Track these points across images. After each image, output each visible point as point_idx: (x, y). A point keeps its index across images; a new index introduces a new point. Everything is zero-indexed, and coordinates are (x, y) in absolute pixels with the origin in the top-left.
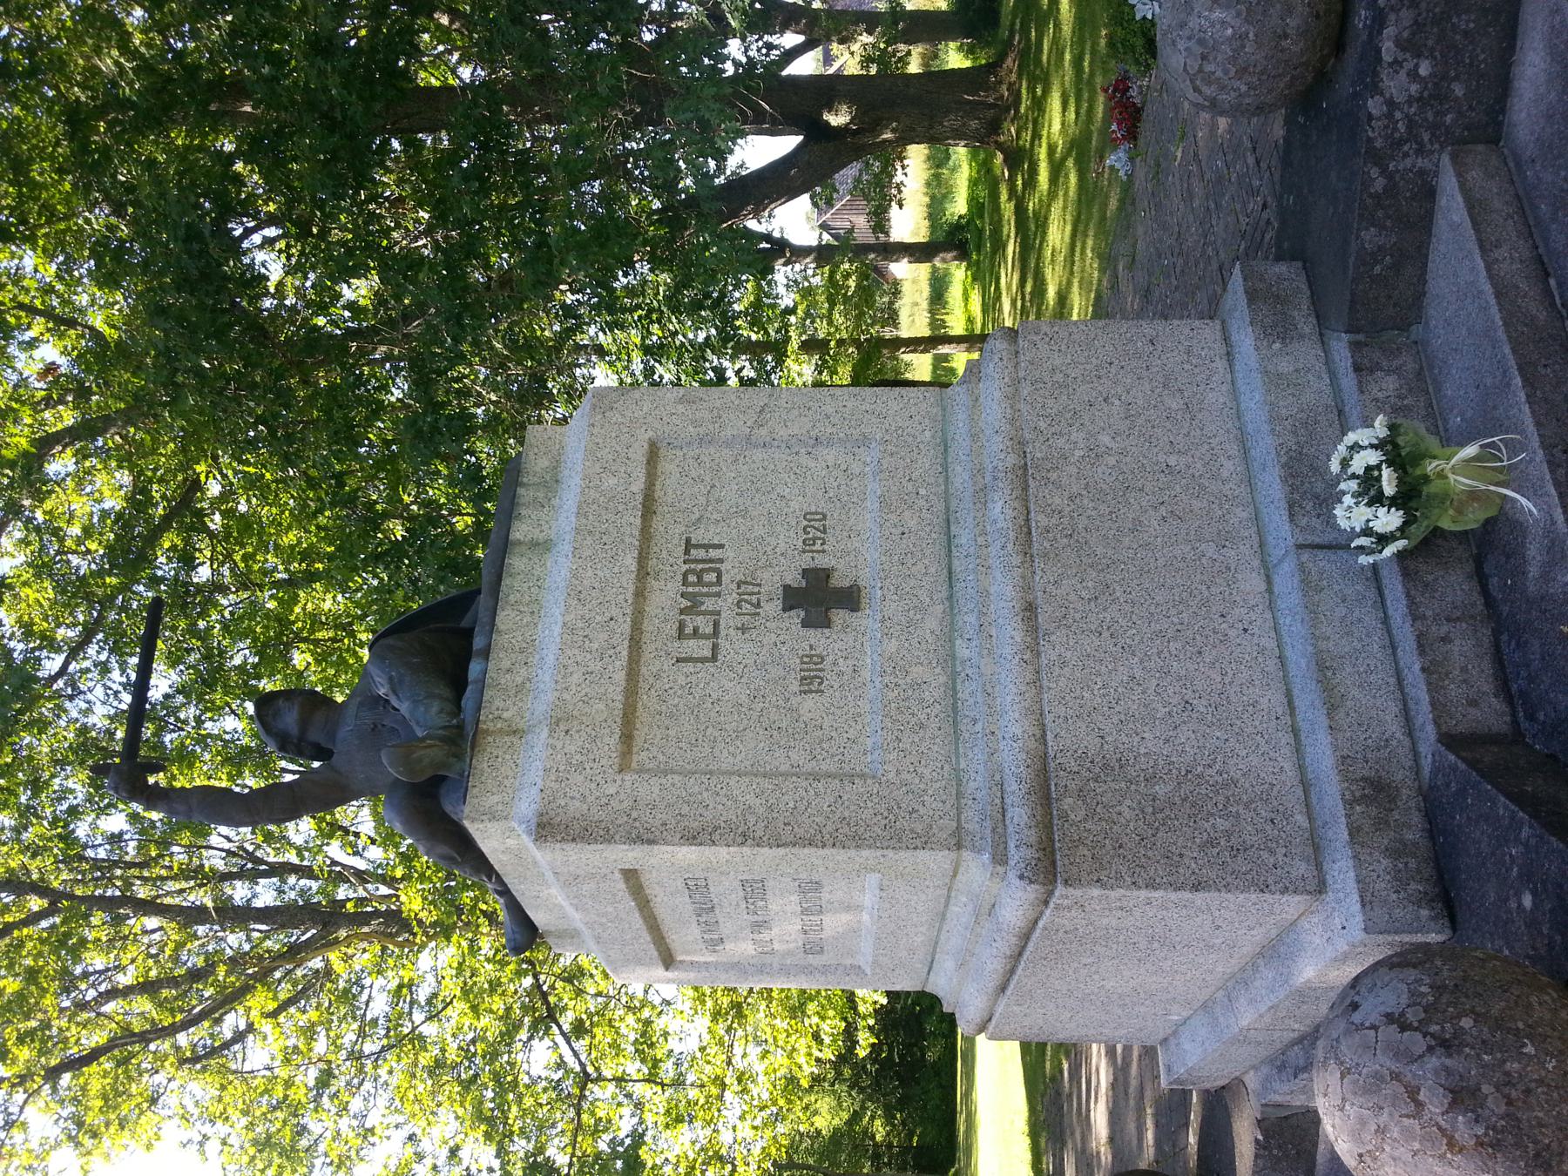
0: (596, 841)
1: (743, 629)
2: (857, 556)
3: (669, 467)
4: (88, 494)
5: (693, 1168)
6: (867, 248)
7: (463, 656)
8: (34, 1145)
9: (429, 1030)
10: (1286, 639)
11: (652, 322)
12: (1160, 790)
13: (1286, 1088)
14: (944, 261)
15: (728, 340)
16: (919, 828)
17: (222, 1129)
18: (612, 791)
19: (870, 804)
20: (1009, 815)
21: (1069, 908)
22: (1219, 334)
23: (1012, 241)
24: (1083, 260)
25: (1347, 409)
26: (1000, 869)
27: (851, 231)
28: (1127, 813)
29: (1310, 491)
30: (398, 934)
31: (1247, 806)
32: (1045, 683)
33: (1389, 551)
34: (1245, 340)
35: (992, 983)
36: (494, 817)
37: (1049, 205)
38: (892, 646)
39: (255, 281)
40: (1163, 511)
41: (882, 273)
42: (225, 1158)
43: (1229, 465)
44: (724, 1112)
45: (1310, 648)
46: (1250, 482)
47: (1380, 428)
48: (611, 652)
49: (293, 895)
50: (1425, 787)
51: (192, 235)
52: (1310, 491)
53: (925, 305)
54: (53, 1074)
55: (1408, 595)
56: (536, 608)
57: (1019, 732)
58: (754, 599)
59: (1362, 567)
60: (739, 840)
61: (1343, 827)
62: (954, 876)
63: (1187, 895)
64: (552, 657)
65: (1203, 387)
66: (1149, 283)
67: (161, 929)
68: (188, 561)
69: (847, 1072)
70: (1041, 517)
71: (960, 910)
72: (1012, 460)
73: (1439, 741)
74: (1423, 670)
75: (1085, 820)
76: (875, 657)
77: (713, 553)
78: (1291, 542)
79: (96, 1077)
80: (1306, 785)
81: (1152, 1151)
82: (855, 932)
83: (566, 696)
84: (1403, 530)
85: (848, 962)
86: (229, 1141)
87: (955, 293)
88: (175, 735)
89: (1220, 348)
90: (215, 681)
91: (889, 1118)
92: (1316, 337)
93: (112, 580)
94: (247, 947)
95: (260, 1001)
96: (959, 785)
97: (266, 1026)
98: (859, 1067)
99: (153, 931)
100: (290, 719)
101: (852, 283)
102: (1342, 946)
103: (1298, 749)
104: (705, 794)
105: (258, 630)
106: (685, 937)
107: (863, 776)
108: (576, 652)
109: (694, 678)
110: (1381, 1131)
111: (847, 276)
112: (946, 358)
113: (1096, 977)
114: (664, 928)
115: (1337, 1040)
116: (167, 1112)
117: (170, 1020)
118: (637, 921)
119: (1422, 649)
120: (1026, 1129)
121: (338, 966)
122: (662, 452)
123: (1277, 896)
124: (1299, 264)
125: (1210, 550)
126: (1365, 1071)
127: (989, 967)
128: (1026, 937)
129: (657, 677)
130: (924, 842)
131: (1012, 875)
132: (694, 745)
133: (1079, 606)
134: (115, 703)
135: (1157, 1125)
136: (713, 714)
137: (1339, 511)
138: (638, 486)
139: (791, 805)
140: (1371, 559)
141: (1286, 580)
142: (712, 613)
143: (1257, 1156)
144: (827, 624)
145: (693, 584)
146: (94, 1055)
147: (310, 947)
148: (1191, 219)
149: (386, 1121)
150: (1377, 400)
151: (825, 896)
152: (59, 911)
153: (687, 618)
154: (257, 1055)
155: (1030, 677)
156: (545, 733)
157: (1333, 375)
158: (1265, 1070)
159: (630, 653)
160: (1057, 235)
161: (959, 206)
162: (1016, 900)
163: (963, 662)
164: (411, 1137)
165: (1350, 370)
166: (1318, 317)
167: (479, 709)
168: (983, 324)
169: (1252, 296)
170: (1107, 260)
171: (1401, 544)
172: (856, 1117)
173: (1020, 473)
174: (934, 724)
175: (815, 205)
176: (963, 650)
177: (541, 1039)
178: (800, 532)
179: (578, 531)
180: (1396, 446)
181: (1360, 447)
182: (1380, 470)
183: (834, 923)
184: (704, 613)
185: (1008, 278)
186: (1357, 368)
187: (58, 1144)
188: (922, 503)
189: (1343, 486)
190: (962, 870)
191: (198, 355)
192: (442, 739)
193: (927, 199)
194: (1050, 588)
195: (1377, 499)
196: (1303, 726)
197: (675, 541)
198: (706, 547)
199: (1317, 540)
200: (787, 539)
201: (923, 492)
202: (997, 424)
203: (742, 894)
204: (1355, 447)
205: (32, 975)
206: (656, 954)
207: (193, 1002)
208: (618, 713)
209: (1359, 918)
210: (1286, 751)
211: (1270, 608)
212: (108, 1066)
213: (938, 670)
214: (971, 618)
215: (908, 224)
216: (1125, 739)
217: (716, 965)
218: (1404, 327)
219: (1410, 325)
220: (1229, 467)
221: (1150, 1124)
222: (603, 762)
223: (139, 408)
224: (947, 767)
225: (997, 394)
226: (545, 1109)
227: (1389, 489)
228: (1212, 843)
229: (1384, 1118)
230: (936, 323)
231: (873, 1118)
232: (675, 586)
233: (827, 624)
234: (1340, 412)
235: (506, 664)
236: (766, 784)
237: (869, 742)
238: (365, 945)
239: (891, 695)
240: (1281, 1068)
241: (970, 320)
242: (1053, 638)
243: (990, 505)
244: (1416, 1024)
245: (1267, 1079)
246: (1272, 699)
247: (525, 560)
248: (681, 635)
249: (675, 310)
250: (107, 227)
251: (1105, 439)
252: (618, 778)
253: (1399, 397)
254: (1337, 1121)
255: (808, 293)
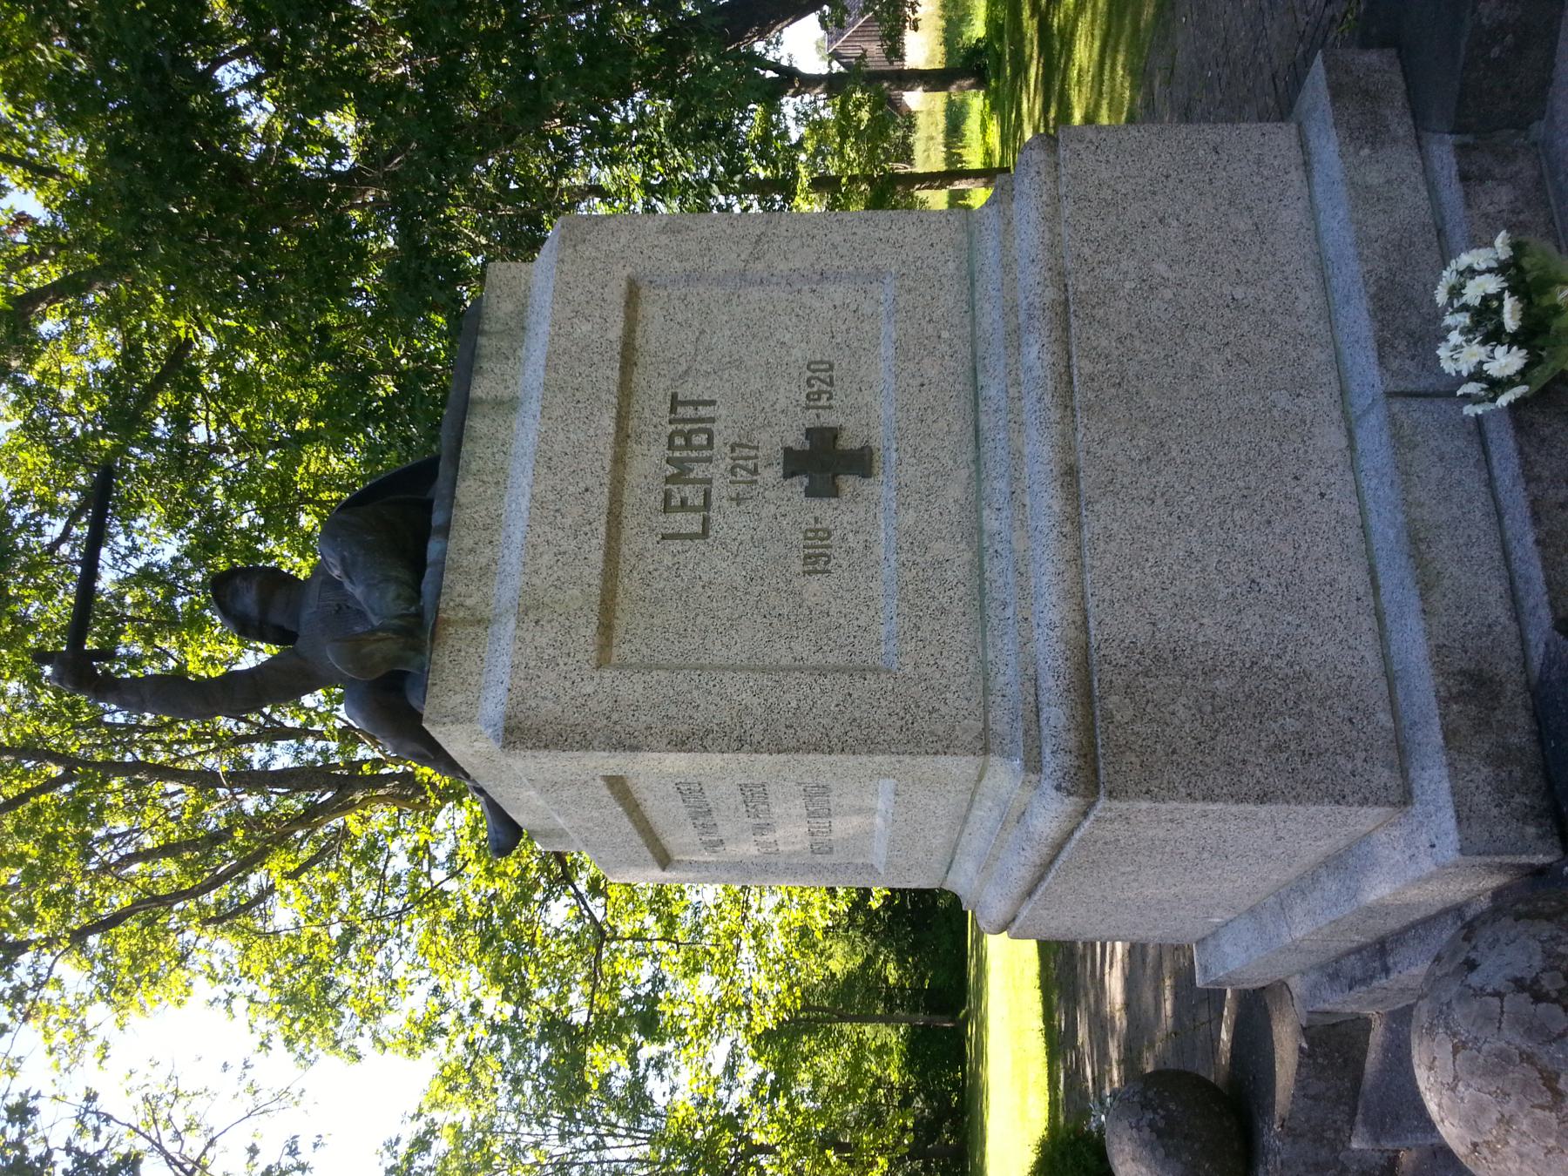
0: (571, 748)
1: (738, 500)
2: (870, 412)
3: (651, 310)
4: (78, 354)
5: (710, 1020)
6: (880, 76)
7: (422, 533)
8: (70, 1000)
9: (452, 886)
10: (1371, 505)
11: (653, 157)
12: (1220, 685)
13: (1339, 998)
14: (961, 89)
15: (734, 177)
16: (940, 729)
17: (247, 987)
18: (589, 689)
19: (883, 703)
20: (1044, 716)
21: (1112, 821)
22: (1294, 141)
23: (1035, 62)
24: (1113, 79)
25: (1448, 227)
26: (1032, 777)
27: (863, 56)
28: (1182, 713)
29: (1406, 327)
30: (413, 796)
31: (1321, 703)
32: (1088, 561)
33: (1503, 401)
34: (1327, 146)
35: (1017, 890)
36: (456, 720)
37: (1076, 20)
38: (909, 518)
39: (224, 116)
40: (1228, 354)
41: (896, 105)
42: (251, 1015)
43: (1305, 297)
44: (740, 966)
45: (1401, 517)
46: (1329, 316)
47: (1501, 246)
48: (587, 529)
49: (311, 756)
50: (1533, 682)
51: (150, 66)
52: (1406, 327)
53: (940, 138)
54: (79, 937)
55: (1521, 452)
56: (501, 478)
57: (1056, 618)
58: (750, 464)
59: (1465, 419)
60: (735, 745)
61: (1437, 728)
62: (980, 779)
63: (1251, 807)
64: (519, 536)
65: (1275, 203)
66: (1190, 99)
67: (181, 791)
68: (182, 421)
69: (861, 919)
70: (1084, 363)
71: (986, 814)
72: (1051, 294)
73: (1555, 628)
74: (1537, 542)
75: (1133, 721)
76: (890, 531)
77: (703, 411)
78: (1380, 389)
79: (126, 939)
80: (1390, 678)
81: (1170, 1021)
82: (869, 834)
83: (536, 581)
84: (1523, 374)
85: (860, 861)
86: (257, 998)
87: (972, 125)
88: (186, 599)
89: (1294, 155)
90: (219, 546)
91: (901, 963)
92: (1411, 140)
93: (106, 443)
94: (266, 808)
95: (277, 863)
96: (986, 679)
97: (288, 886)
98: (872, 915)
99: (174, 794)
100: (249, 600)
101: (865, 115)
102: (1427, 865)
103: (1382, 635)
104: (695, 693)
105: (263, 491)
106: (681, 838)
107: (876, 670)
108: (547, 529)
109: (681, 558)
110: (1505, 1121)
111: (859, 107)
112: (962, 194)
113: (1135, 885)
114: (658, 830)
115: (1449, 1004)
116: (197, 967)
117: (191, 884)
118: (627, 825)
119: (1536, 518)
120: (1038, 983)
121: (355, 828)
122: (644, 292)
123: (1355, 808)
124: (1393, 52)
125: (1283, 399)
126: (1486, 1047)
127: (1016, 874)
128: (1059, 847)
129: (640, 556)
130: (947, 746)
131: (1047, 786)
132: (682, 635)
133: (1128, 469)
134: (124, 568)
135: (1176, 996)
136: (704, 599)
137: (1443, 352)
138: (616, 332)
139: (794, 704)
140: (1479, 410)
141: (1373, 437)
142: (702, 481)
143: (1300, 1065)
144: (834, 492)
145: (680, 448)
146: (117, 919)
147: (329, 810)
148: (1241, 20)
149: (409, 977)
150: (1486, 215)
151: (834, 799)
152: (74, 778)
153: (674, 488)
154: (284, 914)
155: (1069, 552)
156: (512, 624)
157: (1432, 188)
158: (1314, 976)
159: (609, 530)
160: (1083, 53)
161: (977, 29)
162: (1049, 813)
163: (992, 536)
164: (436, 990)
165: (1455, 179)
166: (1414, 116)
167: (438, 595)
168: (1002, 158)
169: (1337, 91)
170: (1140, 75)
171: (1520, 390)
172: (869, 961)
173: (1059, 310)
174: (958, 609)
175: (824, 26)
176: (991, 522)
177: (557, 900)
178: (803, 384)
179: (546, 386)
180: (1520, 269)
181: (1477, 270)
182: (1501, 301)
183: (843, 827)
184: (693, 482)
185: (1030, 103)
186: (1464, 177)
187: (92, 1000)
188: (944, 347)
189: (1449, 320)
190: (988, 774)
191: (169, 200)
192: (399, 631)
193: (943, 23)
194: (1095, 447)
195: (1495, 336)
196: (1391, 610)
197: (660, 398)
198: (696, 404)
199: (1411, 387)
200: (789, 392)
201: (945, 334)
202: (1033, 252)
203: (741, 798)
204: (1471, 272)
205: (50, 842)
206: (650, 856)
207: (215, 869)
208: (596, 599)
209: (1454, 836)
210: (1368, 638)
211: (1352, 468)
212: (136, 926)
213: (962, 546)
214: (1001, 485)
215: (922, 48)
216: (1179, 625)
217: (717, 865)
218: (1521, 123)
219: (1529, 123)
220: (1306, 300)
221: (1168, 994)
222: (579, 656)
223: (115, 264)
224: (972, 659)
225: (1034, 215)
226: (567, 961)
227: (1511, 322)
228: (1279, 747)
229: (1510, 1107)
230: (952, 157)
231: (885, 962)
232: (659, 451)
233: (834, 492)
234: (1440, 232)
235: (468, 542)
236: (765, 681)
237: (883, 630)
238: (382, 806)
239: (908, 576)
240: (1334, 976)
241: (988, 153)
242: (1097, 507)
243: (1024, 349)
244: (1554, 994)
245: (1316, 986)
246: (1353, 577)
247: (488, 421)
248: (667, 507)
249: (678, 142)
250: (62, 60)
251: (1160, 268)
252: (596, 674)
253: (1513, 212)
254: (1445, 1101)
255: (818, 126)
